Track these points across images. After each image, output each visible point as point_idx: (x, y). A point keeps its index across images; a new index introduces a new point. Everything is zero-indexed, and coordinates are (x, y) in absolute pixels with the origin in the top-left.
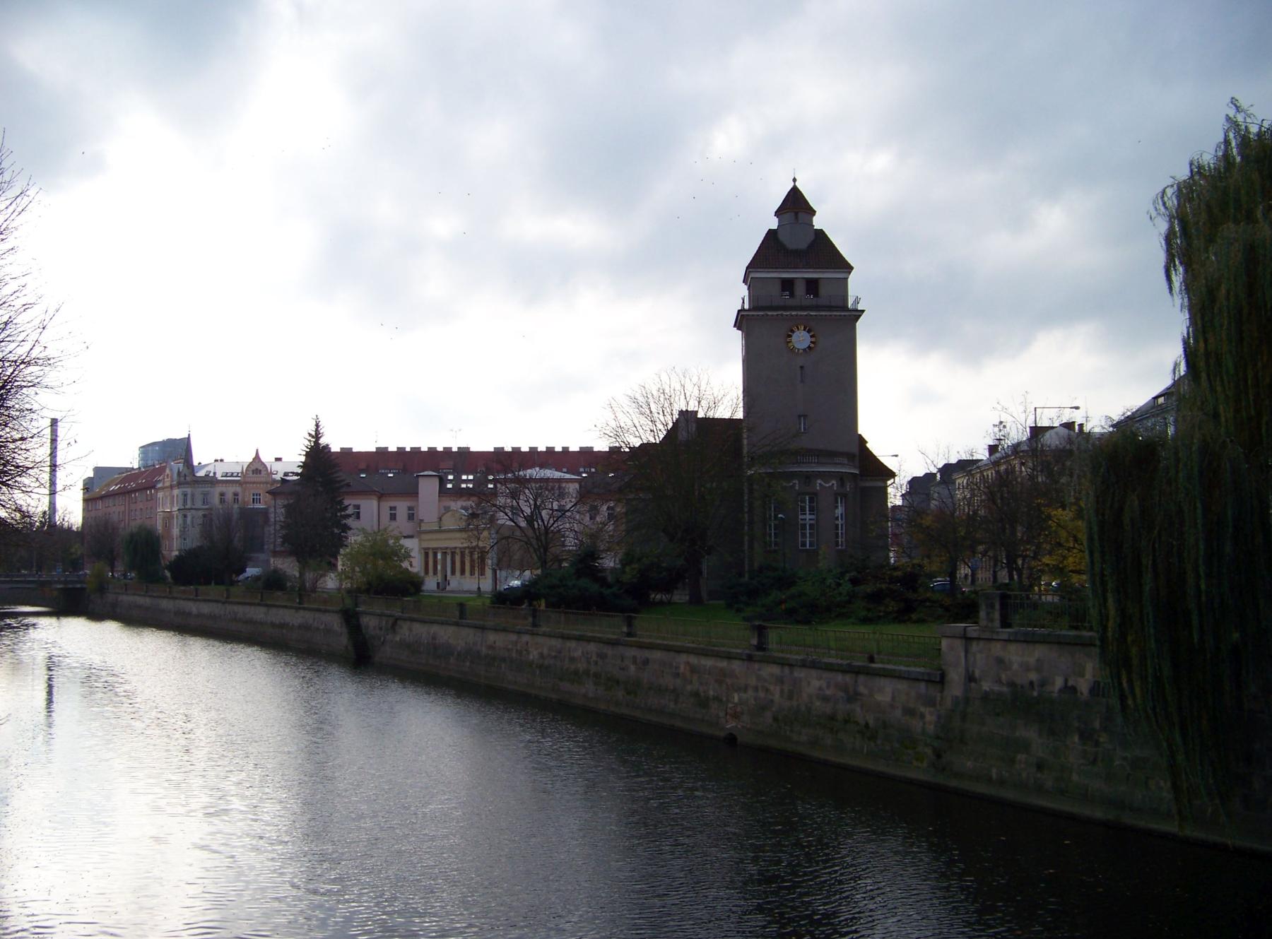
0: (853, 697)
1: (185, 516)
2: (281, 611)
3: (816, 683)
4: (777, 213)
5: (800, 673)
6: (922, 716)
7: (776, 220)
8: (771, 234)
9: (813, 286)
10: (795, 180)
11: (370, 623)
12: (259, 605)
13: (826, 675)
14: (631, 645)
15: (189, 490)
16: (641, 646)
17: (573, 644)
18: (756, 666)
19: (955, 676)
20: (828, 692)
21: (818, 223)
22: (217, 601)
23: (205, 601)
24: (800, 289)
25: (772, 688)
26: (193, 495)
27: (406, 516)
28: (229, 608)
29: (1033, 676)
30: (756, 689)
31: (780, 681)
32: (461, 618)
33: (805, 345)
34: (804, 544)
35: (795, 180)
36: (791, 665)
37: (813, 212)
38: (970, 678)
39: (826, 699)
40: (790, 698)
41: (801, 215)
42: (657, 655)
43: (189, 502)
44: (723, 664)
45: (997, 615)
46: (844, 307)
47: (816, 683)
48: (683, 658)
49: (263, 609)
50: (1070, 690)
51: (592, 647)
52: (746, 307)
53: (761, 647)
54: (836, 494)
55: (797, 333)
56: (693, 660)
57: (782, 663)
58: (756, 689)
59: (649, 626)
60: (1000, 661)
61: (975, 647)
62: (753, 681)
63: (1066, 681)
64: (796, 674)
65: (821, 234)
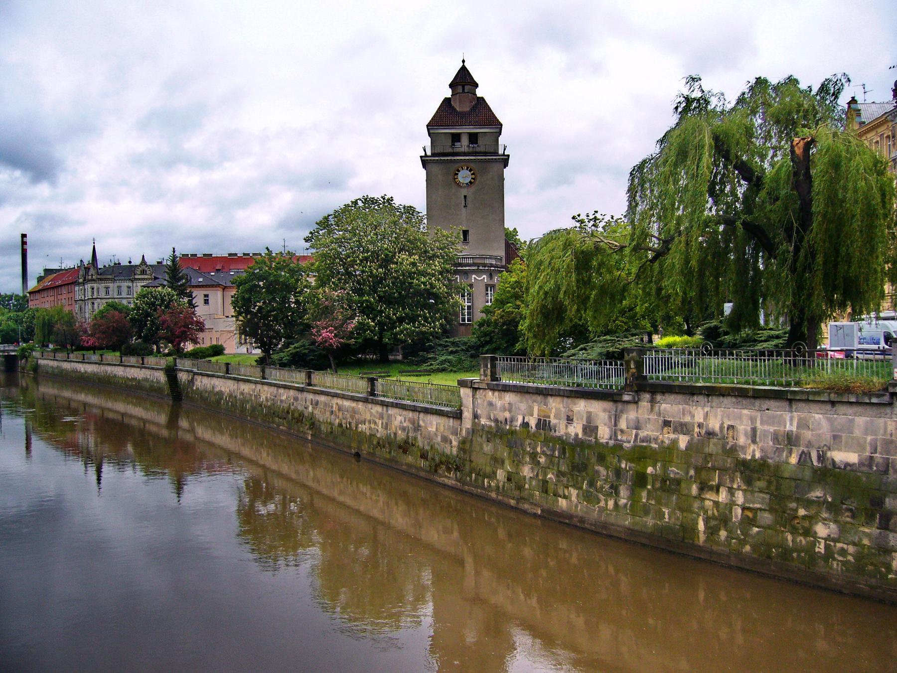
0: (417, 428)
1: (93, 303)
2: (133, 370)
3: (399, 418)
4: (451, 86)
5: (391, 411)
6: (451, 443)
7: (450, 90)
8: (447, 101)
9: (473, 138)
10: (463, 61)
11: (183, 377)
12: (119, 365)
13: (405, 413)
14: (309, 391)
15: (95, 285)
16: (315, 392)
17: (281, 391)
18: (370, 406)
19: (467, 415)
20: (405, 425)
21: (479, 93)
22: (96, 363)
23: (89, 363)
24: (465, 141)
25: (377, 421)
26: (98, 289)
27: (203, 302)
28: (103, 368)
29: (507, 415)
30: (370, 422)
31: (381, 417)
32: (227, 373)
33: (468, 181)
34: (463, 320)
35: (463, 61)
36: (387, 406)
37: (477, 85)
38: (476, 416)
39: (404, 429)
40: (386, 428)
41: (467, 88)
42: (322, 398)
43: (95, 293)
44: (354, 404)
45: (489, 372)
46: (496, 153)
47: (399, 418)
48: (335, 401)
49: (122, 368)
50: (525, 425)
51: (292, 393)
52: (429, 153)
53: (372, 393)
54: (487, 286)
55: (460, 174)
56: (340, 401)
57: (383, 404)
58: (370, 422)
59: (325, 380)
60: (491, 404)
61: (479, 394)
62: (368, 417)
63: (524, 419)
64: (390, 412)
65: (482, 100)
